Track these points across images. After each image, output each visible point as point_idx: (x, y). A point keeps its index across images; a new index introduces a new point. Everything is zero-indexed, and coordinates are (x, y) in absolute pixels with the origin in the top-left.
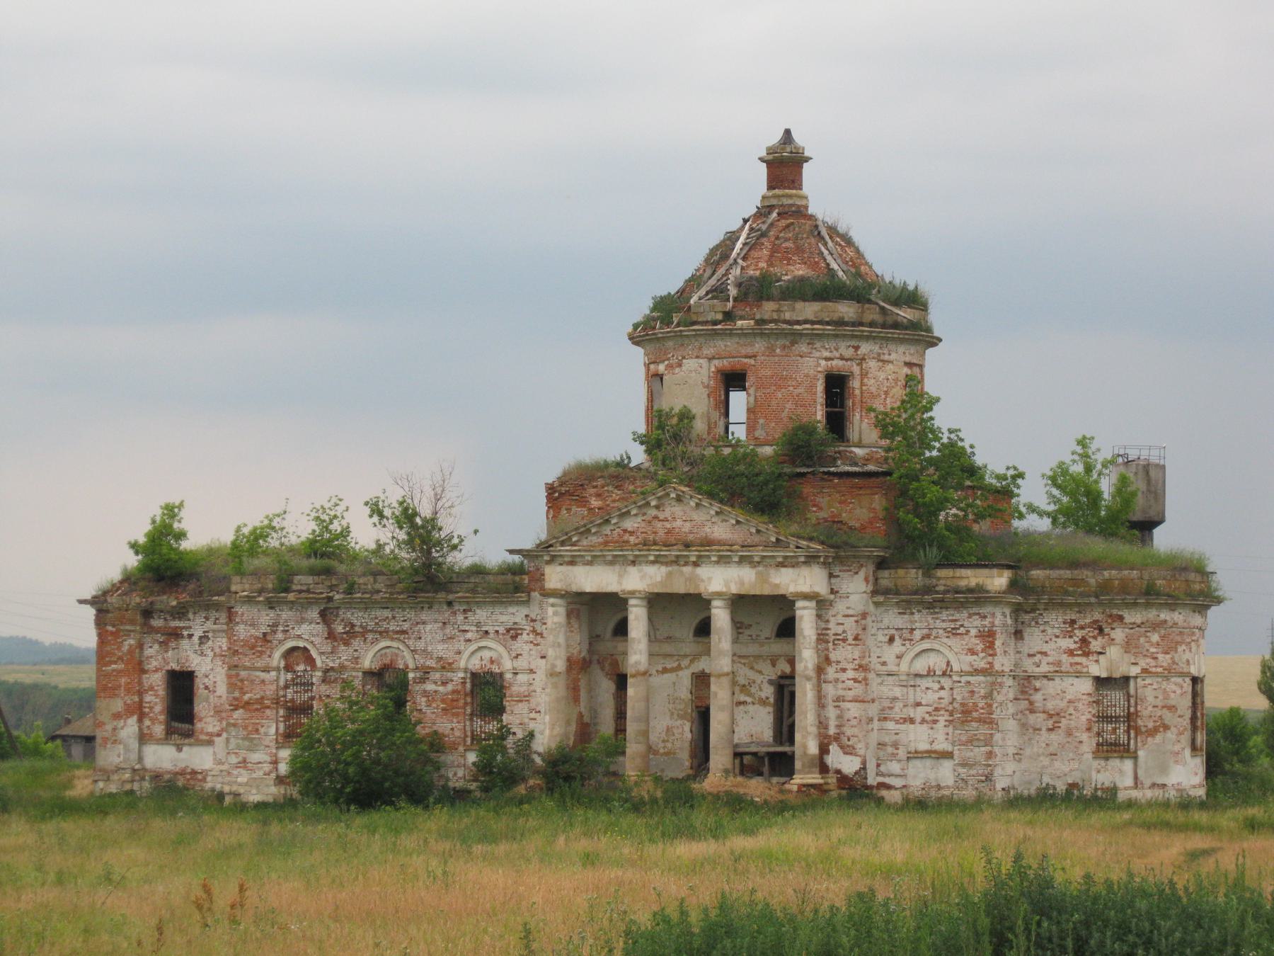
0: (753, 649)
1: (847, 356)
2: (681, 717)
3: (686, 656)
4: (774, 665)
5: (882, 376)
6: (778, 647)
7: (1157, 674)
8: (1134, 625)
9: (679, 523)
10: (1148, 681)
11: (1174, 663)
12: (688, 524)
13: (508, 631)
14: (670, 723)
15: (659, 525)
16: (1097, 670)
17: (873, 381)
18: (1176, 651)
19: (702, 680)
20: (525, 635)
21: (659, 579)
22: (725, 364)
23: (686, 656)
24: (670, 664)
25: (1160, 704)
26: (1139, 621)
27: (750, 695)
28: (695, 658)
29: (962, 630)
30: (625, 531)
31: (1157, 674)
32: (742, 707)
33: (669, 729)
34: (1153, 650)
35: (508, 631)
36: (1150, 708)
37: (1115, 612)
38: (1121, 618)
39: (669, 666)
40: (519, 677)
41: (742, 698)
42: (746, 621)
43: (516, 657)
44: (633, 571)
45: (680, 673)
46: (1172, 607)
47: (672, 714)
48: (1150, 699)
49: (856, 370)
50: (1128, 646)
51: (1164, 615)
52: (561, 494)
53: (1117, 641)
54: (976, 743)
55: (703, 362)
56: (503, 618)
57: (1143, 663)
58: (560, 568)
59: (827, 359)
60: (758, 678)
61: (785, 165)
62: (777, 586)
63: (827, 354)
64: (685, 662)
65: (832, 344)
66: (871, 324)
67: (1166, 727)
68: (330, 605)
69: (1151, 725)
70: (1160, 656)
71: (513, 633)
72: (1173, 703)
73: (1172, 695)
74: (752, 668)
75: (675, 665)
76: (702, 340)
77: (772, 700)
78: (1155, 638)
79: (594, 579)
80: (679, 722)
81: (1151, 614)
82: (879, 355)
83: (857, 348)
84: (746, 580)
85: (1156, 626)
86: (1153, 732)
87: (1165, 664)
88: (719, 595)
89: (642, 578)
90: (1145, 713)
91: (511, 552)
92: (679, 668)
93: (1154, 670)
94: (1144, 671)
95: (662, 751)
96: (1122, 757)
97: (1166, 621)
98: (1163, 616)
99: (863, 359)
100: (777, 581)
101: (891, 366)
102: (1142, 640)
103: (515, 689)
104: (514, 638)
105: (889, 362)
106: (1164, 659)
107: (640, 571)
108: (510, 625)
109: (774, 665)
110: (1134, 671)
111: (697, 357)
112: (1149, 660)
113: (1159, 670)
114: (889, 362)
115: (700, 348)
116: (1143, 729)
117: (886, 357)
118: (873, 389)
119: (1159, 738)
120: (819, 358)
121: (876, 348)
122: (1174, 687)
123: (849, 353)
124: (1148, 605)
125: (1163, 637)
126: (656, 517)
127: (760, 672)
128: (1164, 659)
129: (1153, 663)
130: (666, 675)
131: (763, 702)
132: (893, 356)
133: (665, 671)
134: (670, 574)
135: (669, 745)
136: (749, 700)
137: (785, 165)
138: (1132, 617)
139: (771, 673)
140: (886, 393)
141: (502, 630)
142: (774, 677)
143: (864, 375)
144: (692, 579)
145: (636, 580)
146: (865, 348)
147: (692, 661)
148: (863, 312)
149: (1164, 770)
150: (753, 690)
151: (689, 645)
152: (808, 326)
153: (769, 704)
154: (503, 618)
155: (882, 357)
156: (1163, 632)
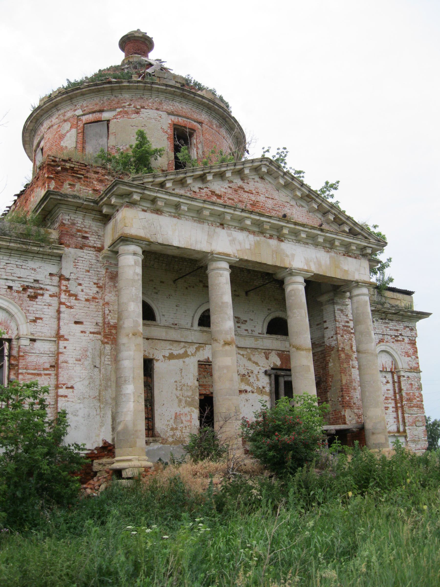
0: (249, 343)
2: (189, 404)
3: (192, 343)
4: (267, 358)
6: (274, 342)
9: (262, 199)
12: (270, 201)
13: (25, 289)
14: (178, 410)
15: (245, 195)
19: (205, 367)
20: (46, 296)
21: (248, 247)
22: (180, 121)
23: (192, 343)
24: (177, 350)
27: (249, 384)
28: (201, 345)
29: (400, 338)
30: (213, 193)
32: (243, 395)
33: (177, 416)
35: (25, 289)
39: (175, 353)
40: (38, 344)
41: (244, 387)
42: (243, 317)
43: (34, 321)
44: (222, 233)
45: (187, 360)
47: (180, 401)
52: (64, 169)
54: (418, 424)
55: (164, 115)
56: (22, 273)
58: (142, 215)
60: (256, 369)
62: (346, 272)
64: (191, 350)
71: (32, 292)
74: (250, 359)
75: (182, 351)
76: (162, 97)
77: (267, 389)
79: (180, 234)
80: (187, 409)
84: (323, 262)
88: (299, 272)
89: (233, 241)
91: (7, 207)
92: (185, 355)
95: (170, 440)
100: (346, 268)
103: (31, 359)
104: (33, 298)
107: (229, 236)
108: (29, 281)
109: (267, 358)
111: (157, 109)
115: (161, 103)
126: (241, 188)
127: (257, 364)
130: (173, 361)
131: (261, 391)
133: (172, 357)
134: (257, 244)
135: (178, 433)
136: (249, 389)
139: (266, 364)
141: (17, 286)
142: (268, 368)
144: (277, 252)
145: (227, 244)
147: (197, 349)
150: (252, 380)
151: (196, 334)
153: (265, 393)
154: (22, 273)
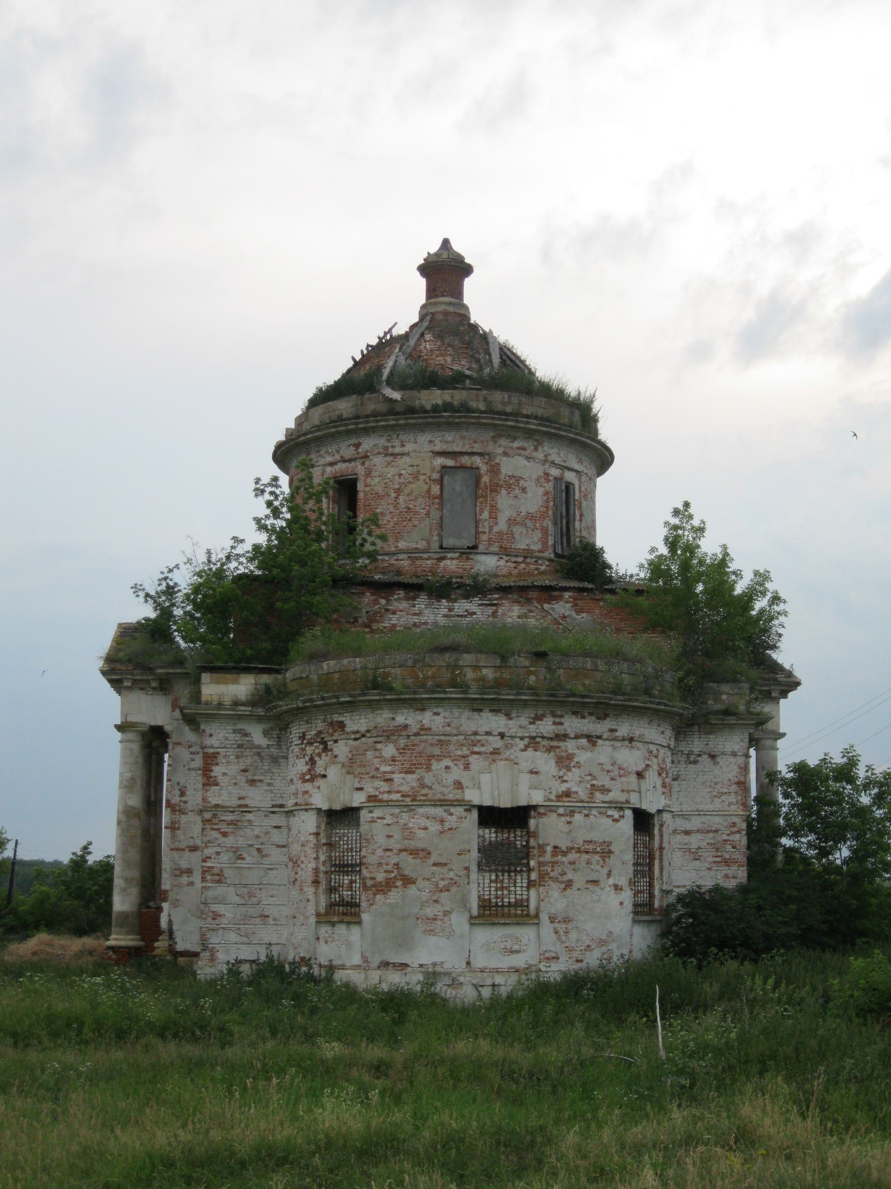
1: (347, 457)
5: (391, 472)
7: (388, 804)
8: (360, 736)
10: (377, 813)
11: (423, 786)
16: (320, 800)
17: (377, 480)
18: (428, 768)
25: (394, 844)
26: (363, 729)
31: (388, 804)
34: (385, 768)
36: (379, 852)
37: (336, 718)
38: (342, 725)
46: (419, 705)
48: (380, 840)
49: (360, 470)
50: (352, 766)
51: (404, 717)
53: (340, 759)
57: (370, 788)
59: (332, 464)
61: (445, 272)
63: (329, 459)
65: (332, 448)
66: (375, 414)
67: (408, 881)
68: (568, 819)
69: (381, 877)
70: (397, 777)
72: (420, 845)
73: (421, 834)
78: (389, 750)
81: (383, 717)
82: (386, 448)
83: (357, 446)
85: (389, 735)
86: (386, 887)
87: (404, 788)
90: (371, 859)
93: (385, 797)
94: (372, 798)
96: (348, 923)
97: (406, 726)
98: (400, 719)
99: (366, 457)
101: (406, 459)
102: (370, 754)
105: (403, 454)
106: (405, 782)
110: (358, 799)
112: (378, 783)
113: (395, 796)
114: (403, 454)
116: (369, 883)
117: (398, 450)
118: (379, 489)
119: (394, 896)
120: (324, 465)
121: (382, 442)
122: (423, 822)
123: (349, 453)
124: (373, 706)
125: (402, 751)
128: (405, 782)
129: (385, 787)
132: (409, 447)
137: (445, 272)
138: (356, 722)
140: (398, 491)
143: (369, 473)
146: (367, 444)
148: (362, 404)
149: (405, 942)
152: (311, 436)
155: (390, 450)
156: (402, 742)
